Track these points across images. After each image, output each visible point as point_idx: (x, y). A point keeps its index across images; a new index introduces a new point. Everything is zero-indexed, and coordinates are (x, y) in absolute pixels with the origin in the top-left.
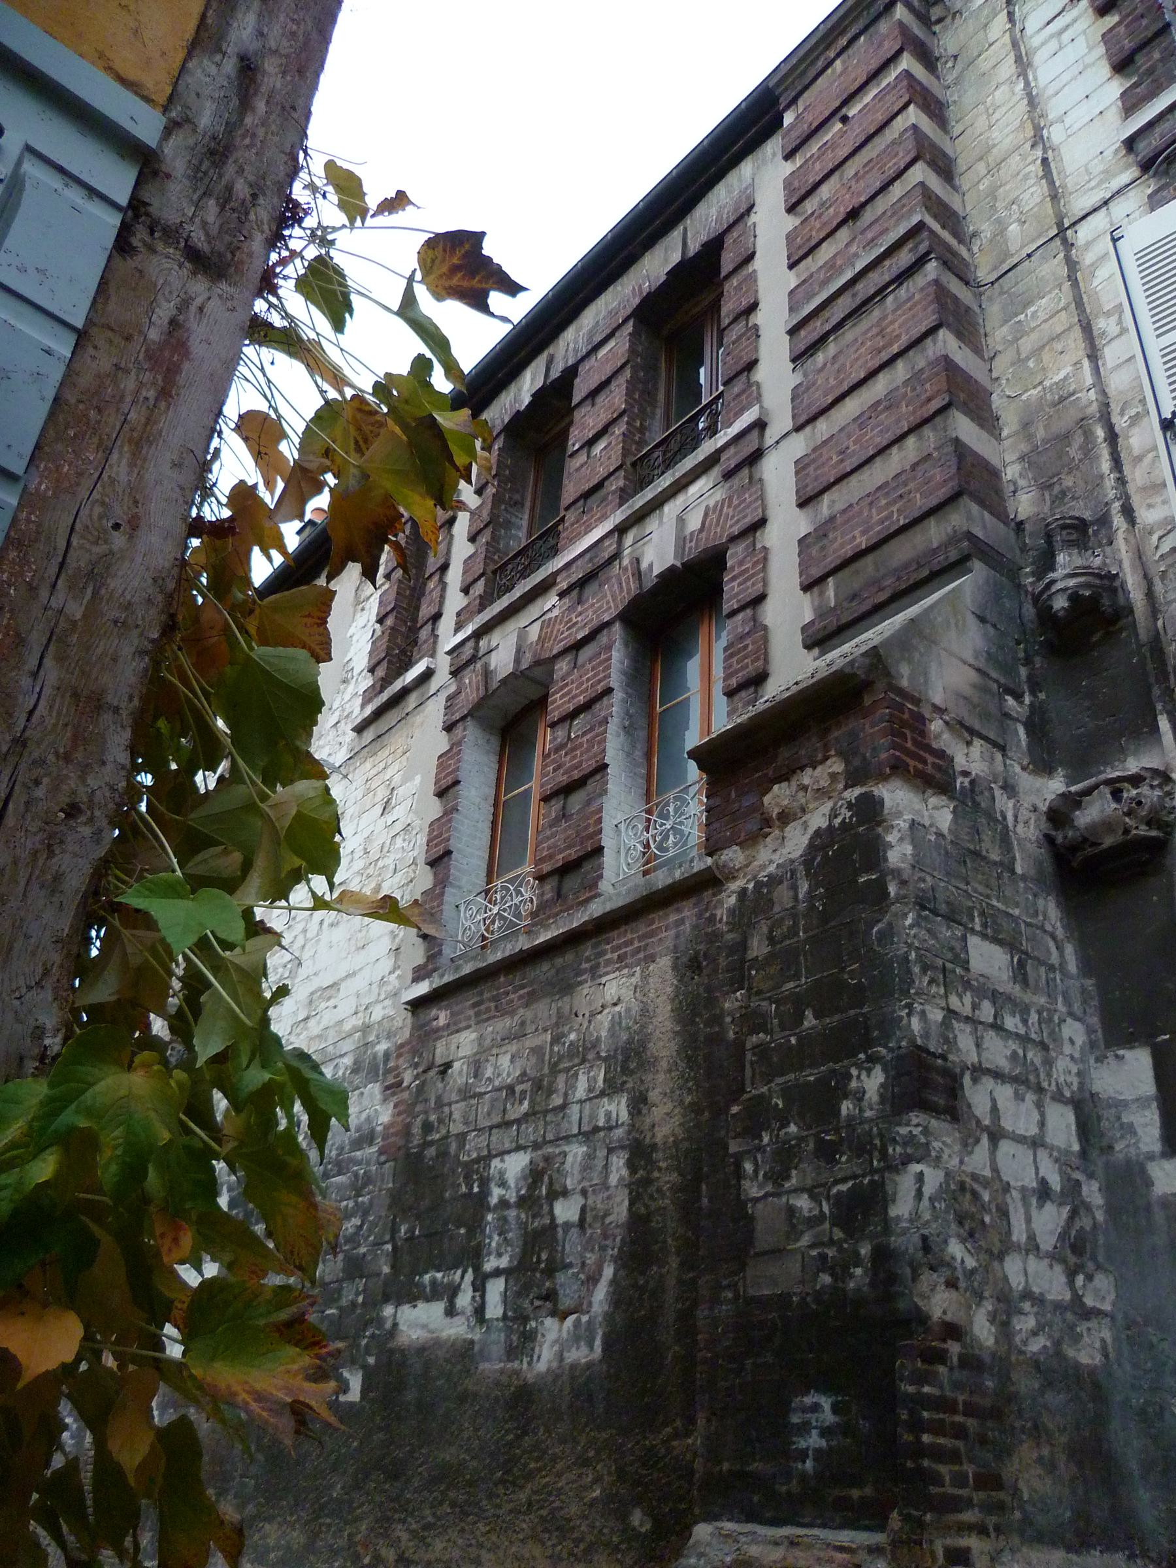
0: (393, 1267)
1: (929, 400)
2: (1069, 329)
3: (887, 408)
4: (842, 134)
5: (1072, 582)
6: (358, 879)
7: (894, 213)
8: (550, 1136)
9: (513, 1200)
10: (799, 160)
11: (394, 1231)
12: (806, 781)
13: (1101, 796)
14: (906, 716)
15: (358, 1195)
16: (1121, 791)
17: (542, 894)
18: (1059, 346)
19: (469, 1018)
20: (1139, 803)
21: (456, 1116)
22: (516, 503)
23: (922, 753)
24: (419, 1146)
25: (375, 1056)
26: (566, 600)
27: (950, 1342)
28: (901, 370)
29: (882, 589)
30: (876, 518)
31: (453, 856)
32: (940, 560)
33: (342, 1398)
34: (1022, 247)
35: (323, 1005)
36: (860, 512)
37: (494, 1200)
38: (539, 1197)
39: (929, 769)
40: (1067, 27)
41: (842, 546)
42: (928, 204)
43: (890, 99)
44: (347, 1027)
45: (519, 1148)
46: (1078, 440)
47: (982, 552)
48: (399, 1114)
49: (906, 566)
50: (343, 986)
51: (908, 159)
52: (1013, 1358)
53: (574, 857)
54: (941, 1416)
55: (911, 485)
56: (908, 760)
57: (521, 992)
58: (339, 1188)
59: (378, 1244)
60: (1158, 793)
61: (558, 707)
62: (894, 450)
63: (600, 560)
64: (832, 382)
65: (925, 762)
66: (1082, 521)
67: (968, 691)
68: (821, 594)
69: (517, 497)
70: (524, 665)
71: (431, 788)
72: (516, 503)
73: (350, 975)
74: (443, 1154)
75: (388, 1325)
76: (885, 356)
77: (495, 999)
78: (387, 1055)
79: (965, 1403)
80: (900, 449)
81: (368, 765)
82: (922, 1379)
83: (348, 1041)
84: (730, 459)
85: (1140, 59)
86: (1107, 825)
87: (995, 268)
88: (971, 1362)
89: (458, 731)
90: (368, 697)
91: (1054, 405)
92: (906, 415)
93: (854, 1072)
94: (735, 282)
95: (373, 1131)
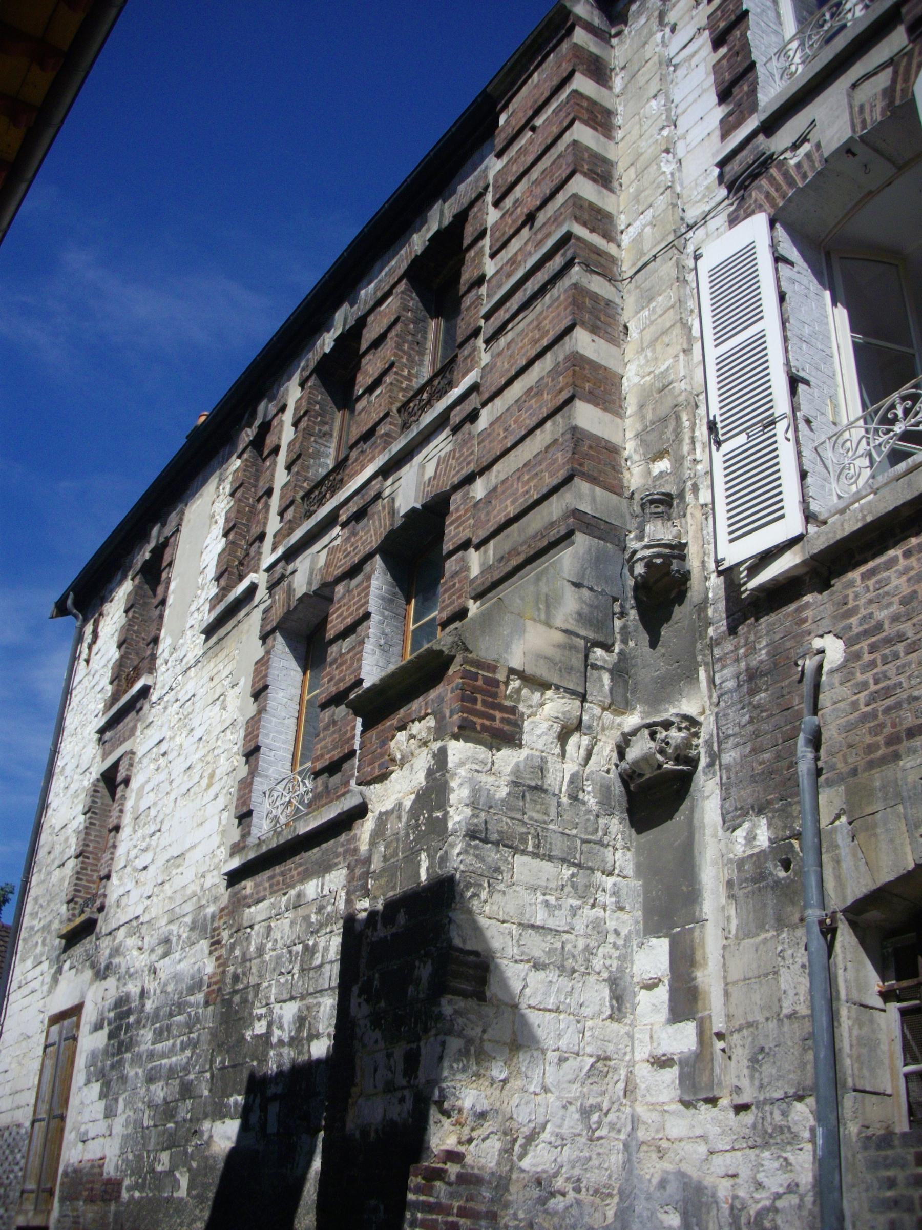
0: (210, 1091)
1: (561, 391)
2: (673, 326)
3: (536, 394)
4: (531, 141)
5: (647, 552)
6: (200, 765)
7: (555, 220)
8: (311, 990)
9: (286, 1040)
10: (505, 159)
11: (212, 1062)
12: (414, 731)
13: (642, 737)
14: (480, 683)
15: (191, 1032)
16: (656, 733)
17: (316, 787)
18: (666, 339)
19: (265, 889)
20: (668, 743)
21: (254, 970)
22: (325, 434)
23: (491, 712)
24: (229, 993)
25: (205, 916)
26: (346, 530)
27: (449, 1164)
28: (547, 362)
29: (519, 554)
30: (521, 491)
31: (263, 750)
32: (554, 534)
33: (175, 1195)
34: (651, 248)
35: (174, 872)
36: (512, 485)
37: (274, 1040)
38: (302, 1039)
39: (497, 724)
40: (695, 53)
41: (499, 513)
42: (578, 213)
43: (562, 114)
44: (189, 891)
45: (292, 998)
46: (672, 424)
47: (588, 525)
48: (219, 966)
49: (535, 536)
50: (187, 856)
51: (568, 171)
52: (514, 1176)
53: (336, 758)
54: (434, 1217)
55: (543, 466)
56: (475, 719)
57: (300, 869)
58: (179, 1025)
59: (202, 1072)
60: (683, 734)
61: (334, 626)
62: (538, 432)
63: (368, 498)
64: (506, 366)
65: (493, 718)
66: (669, 495)
67: (550, 652)
68: (485, 552)
69: (326, 428)
70: (314, 588)
71: (249, 690)
72: (325, 434)
73: (193, 847)
74: (245, 1001)
75: (206, 1137)
76: (538, 348)
77: (283, 874)
78: (213, 917)
79: (460, 1208)
80: (542, 432)
81: (212, 665)
82: (426, 1190)
83: (189, 903)
84: (456, 416)
85: (736, 90)
86: (646, 759)
87: (634, 264)
88: (469, 1180)
89: (270, 641)
90: (216, 600)
91: (660, 391)
92: (548, 401)
93: (417, 963)
94: (472, 253)
95: (201, 980)
